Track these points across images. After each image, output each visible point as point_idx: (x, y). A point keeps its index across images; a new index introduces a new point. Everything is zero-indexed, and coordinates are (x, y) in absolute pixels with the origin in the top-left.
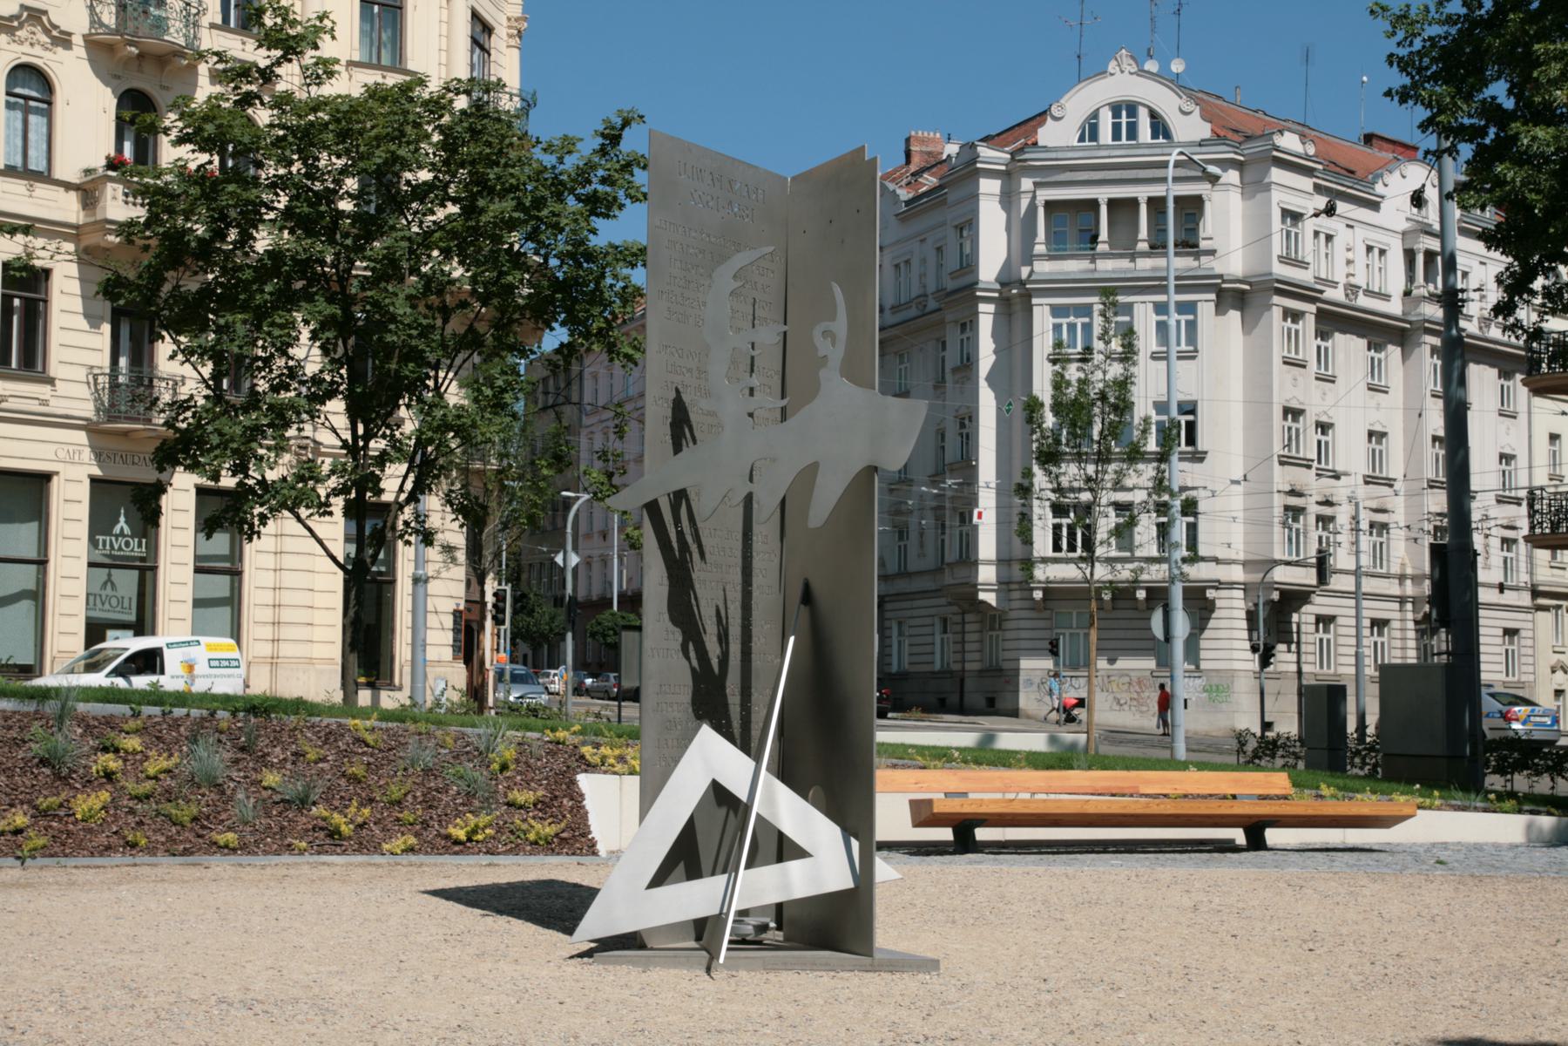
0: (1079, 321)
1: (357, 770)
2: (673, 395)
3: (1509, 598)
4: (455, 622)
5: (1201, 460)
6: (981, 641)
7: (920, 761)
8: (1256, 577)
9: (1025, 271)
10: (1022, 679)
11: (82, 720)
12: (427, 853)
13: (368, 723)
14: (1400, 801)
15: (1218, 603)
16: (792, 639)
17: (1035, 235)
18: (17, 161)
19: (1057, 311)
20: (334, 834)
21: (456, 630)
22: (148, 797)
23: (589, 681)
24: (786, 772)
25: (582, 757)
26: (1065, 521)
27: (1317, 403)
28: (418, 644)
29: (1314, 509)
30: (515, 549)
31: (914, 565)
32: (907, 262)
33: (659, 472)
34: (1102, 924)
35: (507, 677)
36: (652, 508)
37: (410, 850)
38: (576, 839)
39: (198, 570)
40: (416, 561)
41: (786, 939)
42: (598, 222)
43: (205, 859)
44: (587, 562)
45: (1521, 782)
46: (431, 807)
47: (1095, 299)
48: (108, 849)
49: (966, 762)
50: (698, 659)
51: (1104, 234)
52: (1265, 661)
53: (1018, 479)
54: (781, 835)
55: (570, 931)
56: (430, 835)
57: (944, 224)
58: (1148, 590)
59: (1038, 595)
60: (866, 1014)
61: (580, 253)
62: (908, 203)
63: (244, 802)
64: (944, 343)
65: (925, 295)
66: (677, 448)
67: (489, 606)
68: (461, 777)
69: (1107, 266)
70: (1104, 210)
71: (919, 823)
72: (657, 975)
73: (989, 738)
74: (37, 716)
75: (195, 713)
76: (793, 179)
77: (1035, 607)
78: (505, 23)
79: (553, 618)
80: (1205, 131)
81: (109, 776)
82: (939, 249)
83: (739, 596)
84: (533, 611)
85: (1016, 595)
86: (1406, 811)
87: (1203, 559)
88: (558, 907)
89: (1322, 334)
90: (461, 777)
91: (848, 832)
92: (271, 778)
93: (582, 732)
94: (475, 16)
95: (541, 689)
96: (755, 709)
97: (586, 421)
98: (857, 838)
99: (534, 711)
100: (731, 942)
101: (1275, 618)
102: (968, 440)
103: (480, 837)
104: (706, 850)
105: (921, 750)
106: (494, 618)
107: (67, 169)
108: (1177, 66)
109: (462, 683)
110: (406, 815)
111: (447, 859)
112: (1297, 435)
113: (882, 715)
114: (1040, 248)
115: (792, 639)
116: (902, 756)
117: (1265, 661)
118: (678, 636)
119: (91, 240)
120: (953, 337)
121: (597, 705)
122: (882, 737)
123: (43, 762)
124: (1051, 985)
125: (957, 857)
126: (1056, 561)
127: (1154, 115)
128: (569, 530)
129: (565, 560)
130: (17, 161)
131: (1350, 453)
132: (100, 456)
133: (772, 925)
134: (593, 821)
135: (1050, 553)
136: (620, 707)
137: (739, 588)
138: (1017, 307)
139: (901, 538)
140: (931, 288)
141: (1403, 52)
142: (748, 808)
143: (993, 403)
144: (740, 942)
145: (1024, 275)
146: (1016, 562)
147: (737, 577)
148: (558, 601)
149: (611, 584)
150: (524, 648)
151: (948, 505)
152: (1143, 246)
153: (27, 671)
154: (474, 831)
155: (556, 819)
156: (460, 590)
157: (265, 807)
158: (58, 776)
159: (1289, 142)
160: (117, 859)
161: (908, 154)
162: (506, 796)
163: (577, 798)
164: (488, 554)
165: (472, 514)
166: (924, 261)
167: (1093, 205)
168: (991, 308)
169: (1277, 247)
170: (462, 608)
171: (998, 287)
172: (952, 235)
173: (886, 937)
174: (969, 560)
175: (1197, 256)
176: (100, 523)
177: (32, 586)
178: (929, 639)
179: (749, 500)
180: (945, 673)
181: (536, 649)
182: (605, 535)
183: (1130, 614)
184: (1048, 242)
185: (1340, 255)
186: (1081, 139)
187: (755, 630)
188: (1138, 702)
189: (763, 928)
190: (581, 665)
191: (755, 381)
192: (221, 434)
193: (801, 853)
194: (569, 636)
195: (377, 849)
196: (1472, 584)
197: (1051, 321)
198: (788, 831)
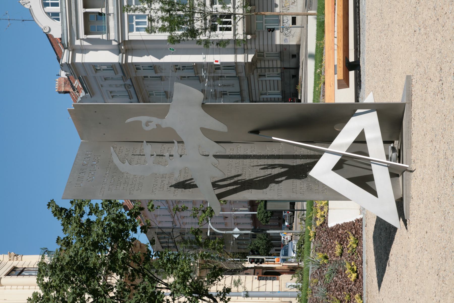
0: (135, 20)
2: (173, 188)
4: (263, 280)
6: (269, 61)
7: (321, 85)
9: (114, 43)
12: (362, 290)
16: (273, 138)
17: (99, 39)
21: (266, 279)
23: (286, 224)
24: (329, 140)
25: (321, 225)
26: (219, 26)
30: (232, 255)
32: (111, 92)
33: (205, 194)
34: (390, 8)
35: (285, 257)
36: (219, 196)
37: (361, 297)
38: (355, 227)
40: (238, 296)
41: (398, 139)
44: (237, 224)
46: (343, 288)
47: (126, 14)
49: (321, 66)
50: (282, 177)
51: (99, 10)
53: (202, 46)
54: (355, 142)
55: (395, 229)
56: (354, 288)
57: (95, 77)
59: (249, 37)
60: (430, 106)
62: (86, 92)
64: (145, 77)
65: (125, 85)
66: (195, 186)
67: (256, 265)
68: (330, 275)
69: (112, 9)
71: (347, 85)
73: (311, 56)
76: (82, 139)
78: (11, 262)
79: (261, 239)
82: (105, 79)
83: (255, 160)
84: (257, 247)
85: (249, 46)
88: (385, 235)
90: (330, 275)
91: (353, 114)
93: (311, 226)
94: (8, 274)
95: (290, 243)
96: (302, 153)
97: (178, 226)
98: (356, 110)
99: (300, 246)
100: (399, 162)
103: (355, 268)
105: (316, 84)
106: (261, 263)
109: (290, 276)
110: (347, 298)
111: (364, 281)
113: (300, 101)
115: (273, 138)
116: (319, 90)
118: (272, 185)
120: (142, 73)
121: (297, 220)
122: (310, 100)
124: (417, 29)
125: (362, 69)
126: (235, 30)
128: (224, 232)
129: (236, 234)
133: (392, 145)
134: (348, 221)
135: (232, 32)
136: (297, 210)
137: (252, 160)
138: (129, 46)
139: (226, 94)
140: (121, 82)
142: (344, 156)
143: (170, 56)
145: (116, 43)
146: (235, 46)
147: (247, 161)
148: (254, 236)
149: (246, 215)
150: (273, 251)
151: (212, 75)
154: (353, 270)
155: (347, 236)
156: (249, 277)
161: (66, 92)
162: (338, 257)
163: (338, 227)
164: (235, 267)
165: (216, 274)
166: (110, 86)
167: (86, 15)
168: (130, 57)
170: (257, 277)
171: (121, 54)
173: (395, 97)
174: (234, 66)
178: (268, 82)
179: (216, 156)
180: (282, 75)
181: (273, 246)
184: (102, 34)
186: (58, 19)
187: (270, 153)
189: (393, 149)
190: (280, 226)
191: (167, 154)
193: (362, 134)
194: (268, 232)
198: (353, 139)
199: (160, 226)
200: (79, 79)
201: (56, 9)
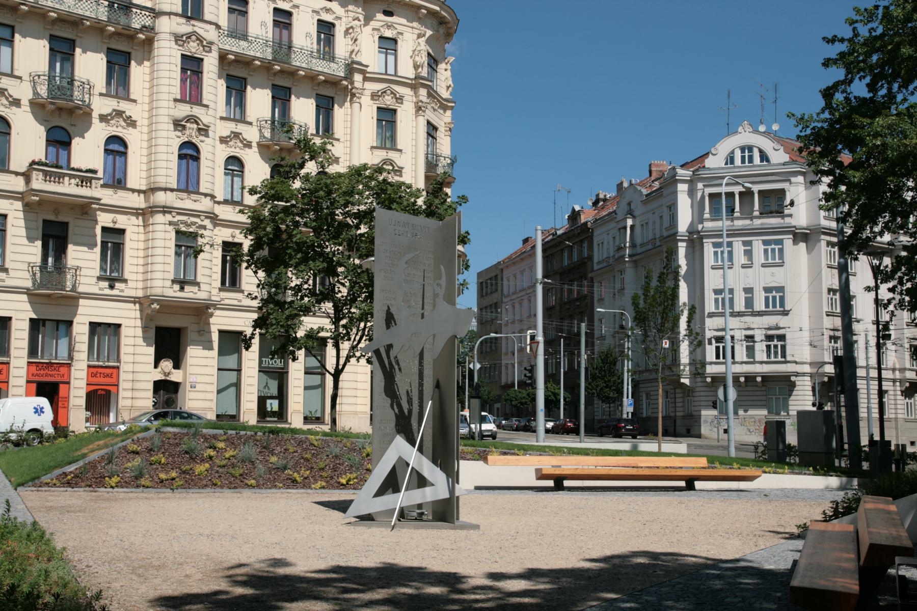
1: (308, 456)
5: (787, 314)
7: (516, 451)
8: (815, 370)
9: (700, 227)
10: (702, 419)
13: (317, 437)
15: (797, 383)
18: (229, 197)
20: (294, 481)
22: (224, 466)
37: (323, 488)
39: (306, 373)
43: (242, 490)
48: (206, 486)
51: (737, 208)
56: (332, 482)
58: (762, 377)
59: (709, 380)
62: (646, 196)
63: (261, 468)
66: (388, 327)
70: (737, 197)
74: (187, 434)
75: (249, 433)
77: (708, 385)
80: (786, 158)
81: (211, 458)
82: (661, 217)
86: (757, 474)
87: (789, 362)
91: (448, 476)
97: (505, 300)
103: (351, 483)
108: (775, 127)
114: (707, 216)
118: (389, 401)
123: (186, 452)
127: (761, 151)
130: (229, 197)
135: (714, 360)
138: (697, 244)
140: (658, 235)
141: (803, 134)
146: (698, 366)
147: (416, 378)
152: (756, 213)
153: (233, 417)
154: (349, 480)
157: (270, 470)
158: (191, 458)
160: (208, 490)
161: (650, 172)
166: (654, 223)
168: (684, 244)
173: (465, 514)
175: (783, 217)
177: (235, 381)
183: (756, 388)
184: (711, 212)
186: (726, 164)
192: (276, 319)
196: (854, 377)
197: (713, 250)
199: (505, 280)
200: (660, 188)
201: (738, 161)
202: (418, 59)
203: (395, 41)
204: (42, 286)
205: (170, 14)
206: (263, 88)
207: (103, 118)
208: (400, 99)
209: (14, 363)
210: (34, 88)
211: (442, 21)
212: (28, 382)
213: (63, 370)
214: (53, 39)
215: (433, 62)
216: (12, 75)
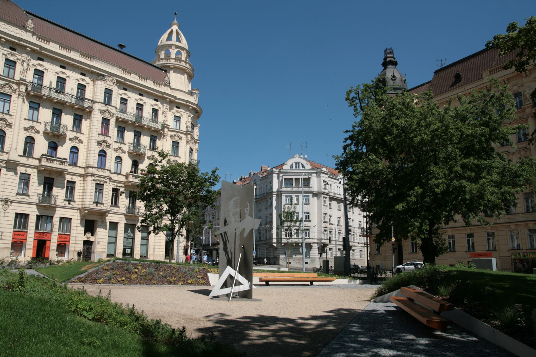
1: (174, 272)
3: (360, 245)
8: (319, 241)
11: (132, 264)
14: (334, 278)
19: (286, 196)
20: (170, 282)
24: (240, 272)
27: (329, 212)
28: (178, 252)
29: (329, 230)
31: (262, 239)
36: (221, 234)
38: (207, 283)
42: (212, 187)
45: (356, 275)
51: (294, 184)
52: (321, 256)
61: (209, 191)
72: (221, 301)
74: (125, 263)
77: (282, 246)
80: (310, 167)
81: (136, 272)
88: (207, 293)
89: (330, 201)
91: (249, 281)
92: (161, 273)
94: (190, 148)
101: (322, 248)
102: (271, 218)
104: (228, 284)
105: (261, 270)
107: (124, 173)
108: (306, 156)
112: (326, 217)
114: (283, 186)
116: (258, 271)
117: (321, 256)
119: (126, 184)
120: (269, 200)
122: (254, 268)
127: (302, 164)
130: (116, 171)
131: (335, 221)
132: (126, 220)
144: (233, 297)
146: (279, 239)
155: (205, 280)
159: (324, 169)
163: (208, 277)
165: (188, 231)
167: (292, 179)
169: (322, 187)
172: (269, 183)
173: (254, 296)
174: (271, 238)
176: (126, 231)
182: (209, 233)
185: (333, 188)
188: (300, 263)
193: (242, 284)
195: (177, 284)
201: (294, 167)
202: (188, 124)
203: (180, 117)
204: (42, 202)
205: (99, 103)
206: (48, 109)
207: (71, 139)
208: (181, 139)
209: (29, 232)
210: (45, 127)
211: (197, 112)
212: (34, 239)
213: (48, 235)
214: (54, 109)
215: (193, 126)
216: (37, 122)
